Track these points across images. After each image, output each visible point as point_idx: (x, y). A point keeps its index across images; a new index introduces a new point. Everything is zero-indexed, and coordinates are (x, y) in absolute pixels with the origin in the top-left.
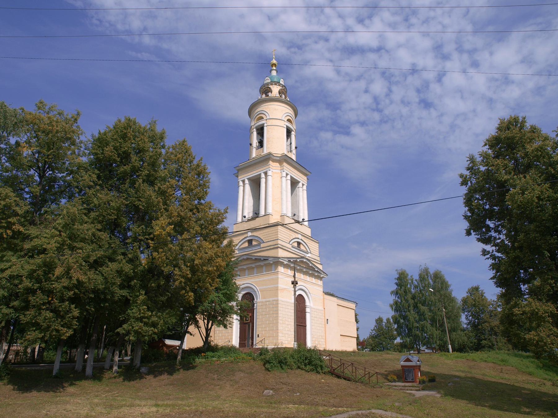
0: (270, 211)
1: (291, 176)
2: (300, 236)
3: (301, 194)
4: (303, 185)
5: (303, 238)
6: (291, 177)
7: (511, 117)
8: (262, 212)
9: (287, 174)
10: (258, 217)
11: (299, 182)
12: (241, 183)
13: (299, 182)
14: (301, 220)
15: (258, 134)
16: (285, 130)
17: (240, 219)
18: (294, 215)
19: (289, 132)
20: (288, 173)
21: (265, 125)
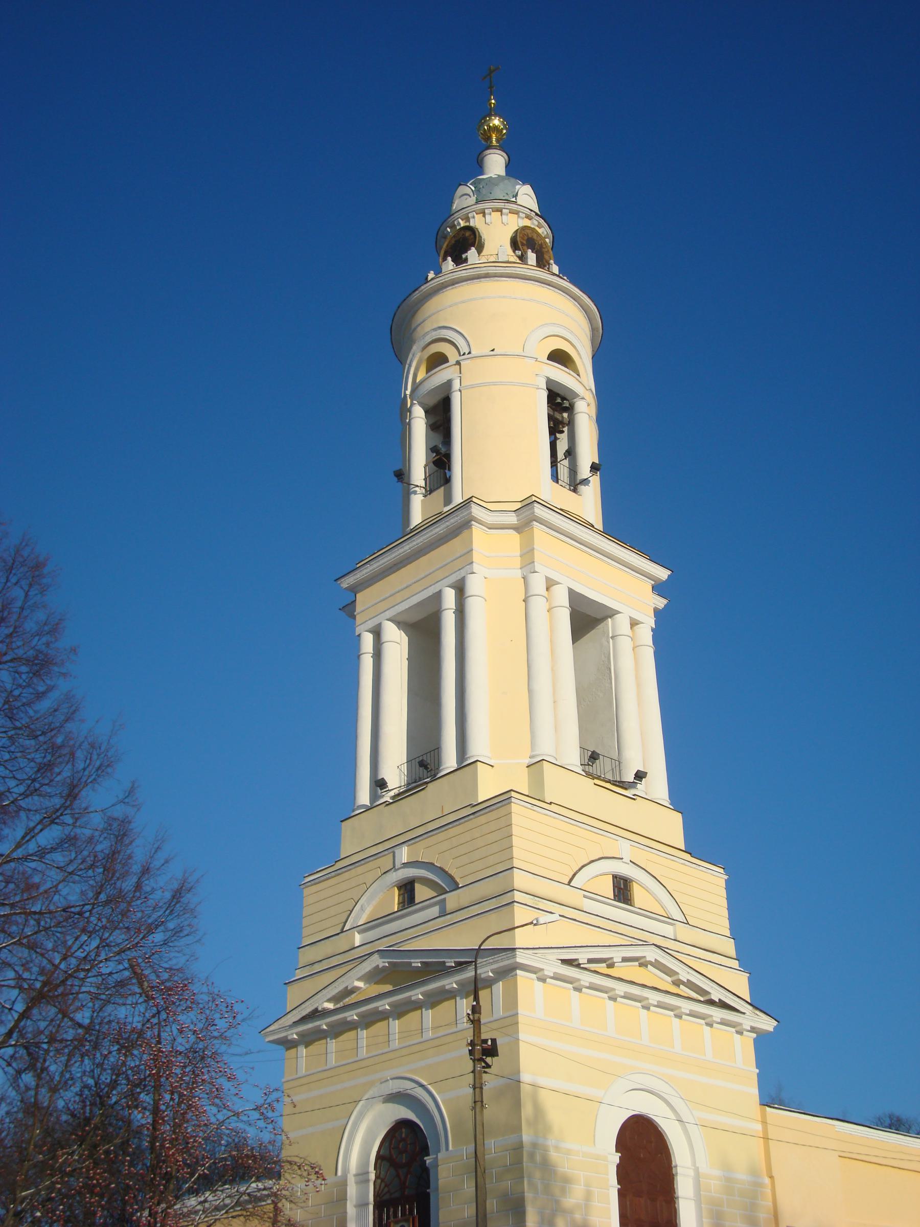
0: (478, 748)
1: (572, 594)
2: (625, 849)
3: (625, 644)
4: (634, 623)
5: (643, 857)
6: (572, 594)
7: (729, 1182)
8: (450, 760)
9: (550, 584)
10: (434, 778)
11: (611, 613)
12: (368, 641)
13: (611, 613)
14: (631, 778)
15: (436, 751)
16: (545, 394)
17: (364, 796)
18: (594, 757)
19: (559, 404)
20: (554, 576)
21: (456, 385)
